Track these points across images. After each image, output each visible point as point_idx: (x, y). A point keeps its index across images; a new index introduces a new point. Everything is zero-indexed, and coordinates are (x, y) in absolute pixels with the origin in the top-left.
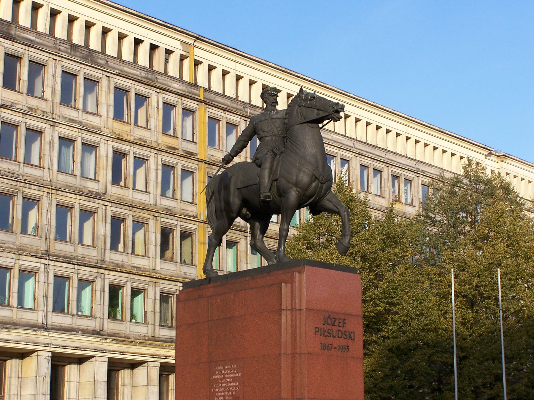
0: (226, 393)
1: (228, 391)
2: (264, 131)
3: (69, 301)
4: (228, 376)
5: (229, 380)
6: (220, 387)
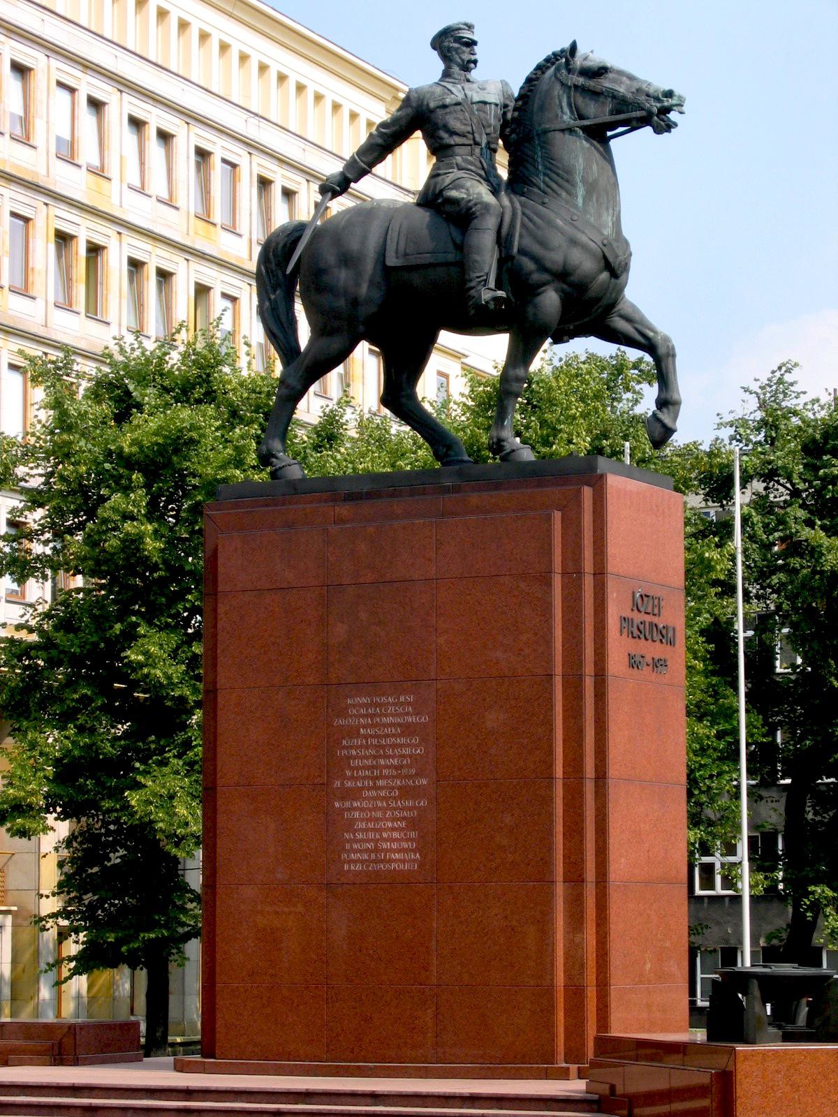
0: (382, 762)
1: (386, 757)
2: (452, 133)
3: (179, 55)
4: (390, 720)
5: (388, 731)
6: (361, 746)
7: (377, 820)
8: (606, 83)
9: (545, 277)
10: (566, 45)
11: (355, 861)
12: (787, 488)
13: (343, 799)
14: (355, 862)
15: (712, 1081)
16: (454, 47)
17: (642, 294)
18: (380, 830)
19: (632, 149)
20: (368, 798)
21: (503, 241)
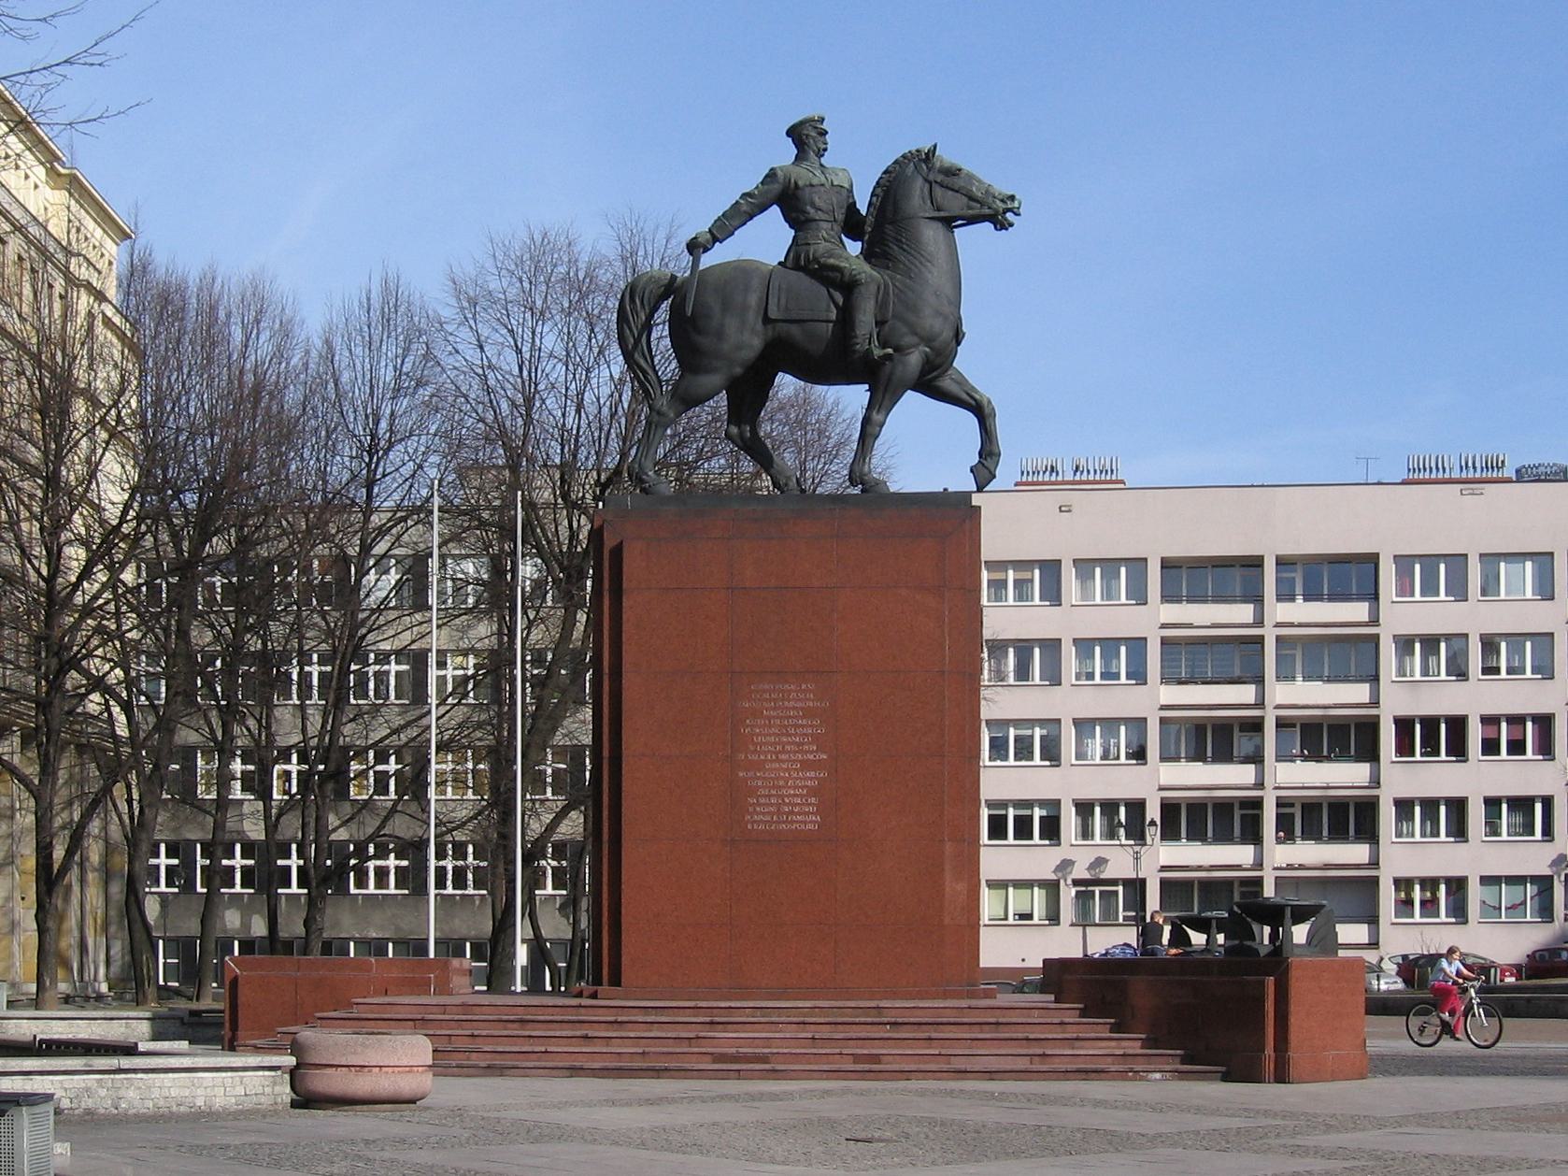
7: (780, 787)
8: (958, 182)
9: (914, 340)
10: (926, 147)
11: (760, 818)
12: (179, 551)
13: (747, 770)
14: (758, 822)
15: (418, 1023)
16: (806, 136)
17: (968, 364)
18: (782, 797)
19: (973, 241)
20: (771, 770)
21: (882, 305)
